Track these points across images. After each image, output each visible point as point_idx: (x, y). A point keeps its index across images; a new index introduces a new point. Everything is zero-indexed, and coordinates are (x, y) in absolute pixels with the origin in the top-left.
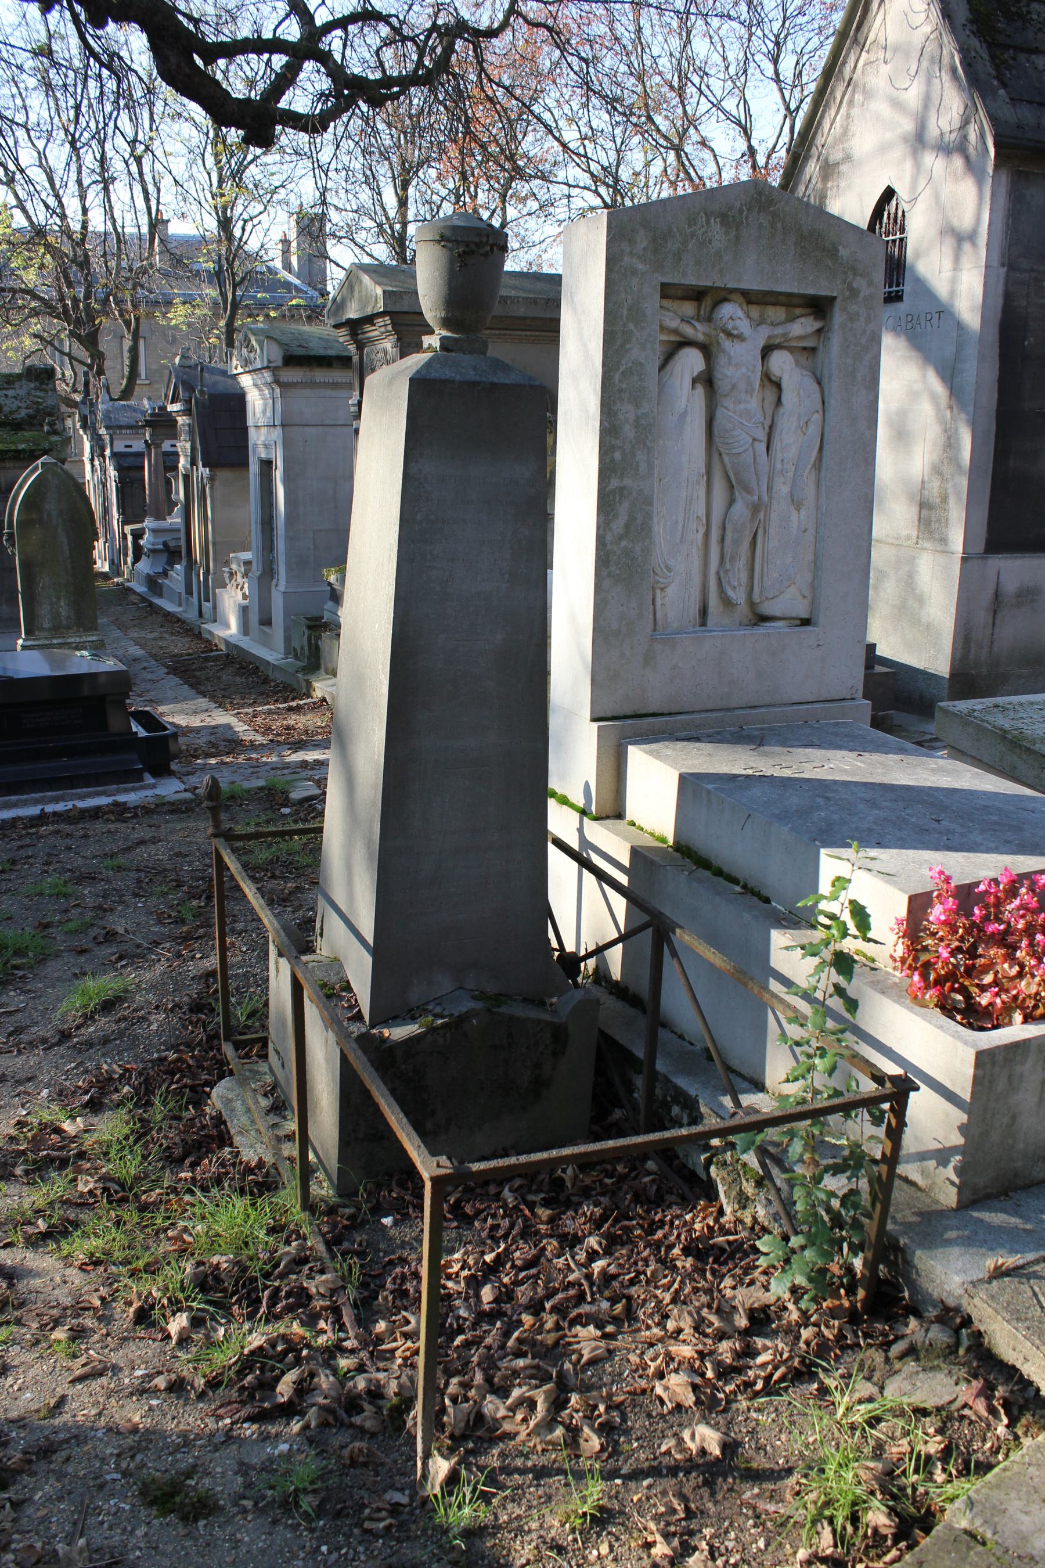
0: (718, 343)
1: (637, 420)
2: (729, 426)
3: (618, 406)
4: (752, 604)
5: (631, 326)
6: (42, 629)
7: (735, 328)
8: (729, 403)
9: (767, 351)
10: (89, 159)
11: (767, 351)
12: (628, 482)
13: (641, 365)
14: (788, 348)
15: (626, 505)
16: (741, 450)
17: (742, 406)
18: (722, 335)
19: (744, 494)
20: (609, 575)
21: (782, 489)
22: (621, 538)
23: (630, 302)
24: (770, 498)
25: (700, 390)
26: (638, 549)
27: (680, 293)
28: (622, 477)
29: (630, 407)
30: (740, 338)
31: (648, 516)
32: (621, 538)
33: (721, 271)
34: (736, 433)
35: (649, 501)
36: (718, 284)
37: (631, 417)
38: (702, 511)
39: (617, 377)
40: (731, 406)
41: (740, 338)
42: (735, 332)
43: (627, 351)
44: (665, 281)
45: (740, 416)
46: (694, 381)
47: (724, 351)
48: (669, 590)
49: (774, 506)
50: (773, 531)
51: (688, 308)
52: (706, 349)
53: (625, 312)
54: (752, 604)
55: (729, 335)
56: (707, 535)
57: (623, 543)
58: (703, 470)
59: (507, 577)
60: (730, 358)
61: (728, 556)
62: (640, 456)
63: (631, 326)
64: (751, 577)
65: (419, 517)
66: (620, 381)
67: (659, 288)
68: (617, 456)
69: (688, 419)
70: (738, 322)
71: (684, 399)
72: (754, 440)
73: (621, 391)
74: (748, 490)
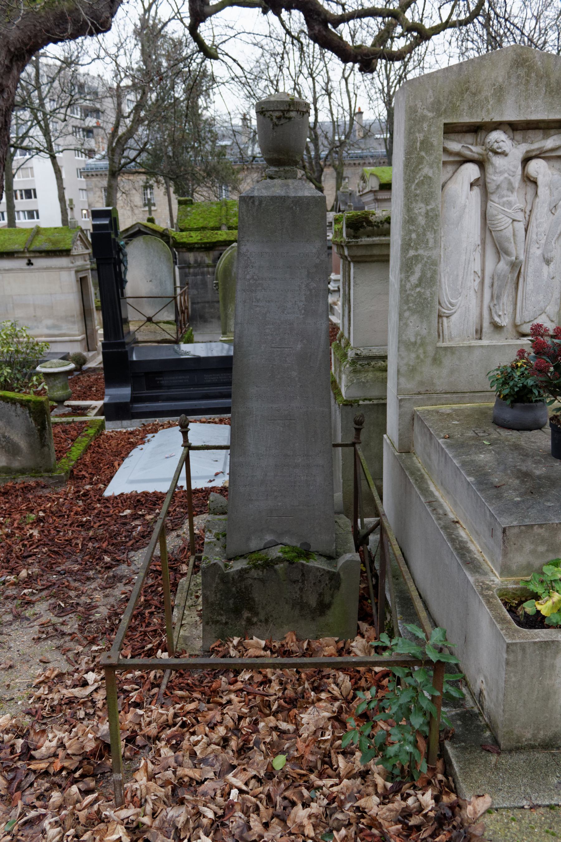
0: (489, 159)
1: (427, 213)
2: (495, 212)
3: (414, 205)
4: (516, 326)
5: (423, 153)
6: (231, 332)
7: (500, 148)
8: (494, 198)
9: (526, 160)
10: (321, 80)
11: (526, 160)
12: (421, 252)
13: (430, 178)
14: (543, 158)
15: (420, 266)
16: (502, 228)
17: (505, 199)
18: (490, 153)
19: (505, 256)
20: (409, 309)
21: (536, 252)
22: (417, 286)
23: (422, 138)
24: (527, 258)
25: (477, 190)
26: (428, 293)
27: (464, 129)
28: (417, 249)
29: (422, 205)
30: (504, 154)
31: (435, 272)
32: (417, 286)
33: (488, 111)
34: (499, 217)
35: (435, 263)
36: (487, 119)
37: (423, 211)
38: (478, 269)
39: (413, 187)
40: (496, 200)
41: (504, 154)
42: (499, 151)
43: (420, 170)
44: (446, 121)
45: (503, 206)
46: (472, 185)
47: (492, 164)
48: (453, 318)
49: (531, 263)
50: (529, 280)
51: (469, 138)
52: (481, 163)
53: (418, 144)
54: (516, 326)
55: (496, 153)
56: (482, 283)
57: (418, 290)
58: (479, 242)
59: (303, 311)
60: (495, 168)
61: (495, 296)
62: (430, 236)
63: (423, 153)
64: (515, 309)
65: (248, 277)
66: (415, 189)
67: (442, 126)
68: (414, 236)
69: (467, 210)
70: (501, 144)
71: (464, 197)
72: (514, 220)
73: (416, 195)
74: (507, 253)
